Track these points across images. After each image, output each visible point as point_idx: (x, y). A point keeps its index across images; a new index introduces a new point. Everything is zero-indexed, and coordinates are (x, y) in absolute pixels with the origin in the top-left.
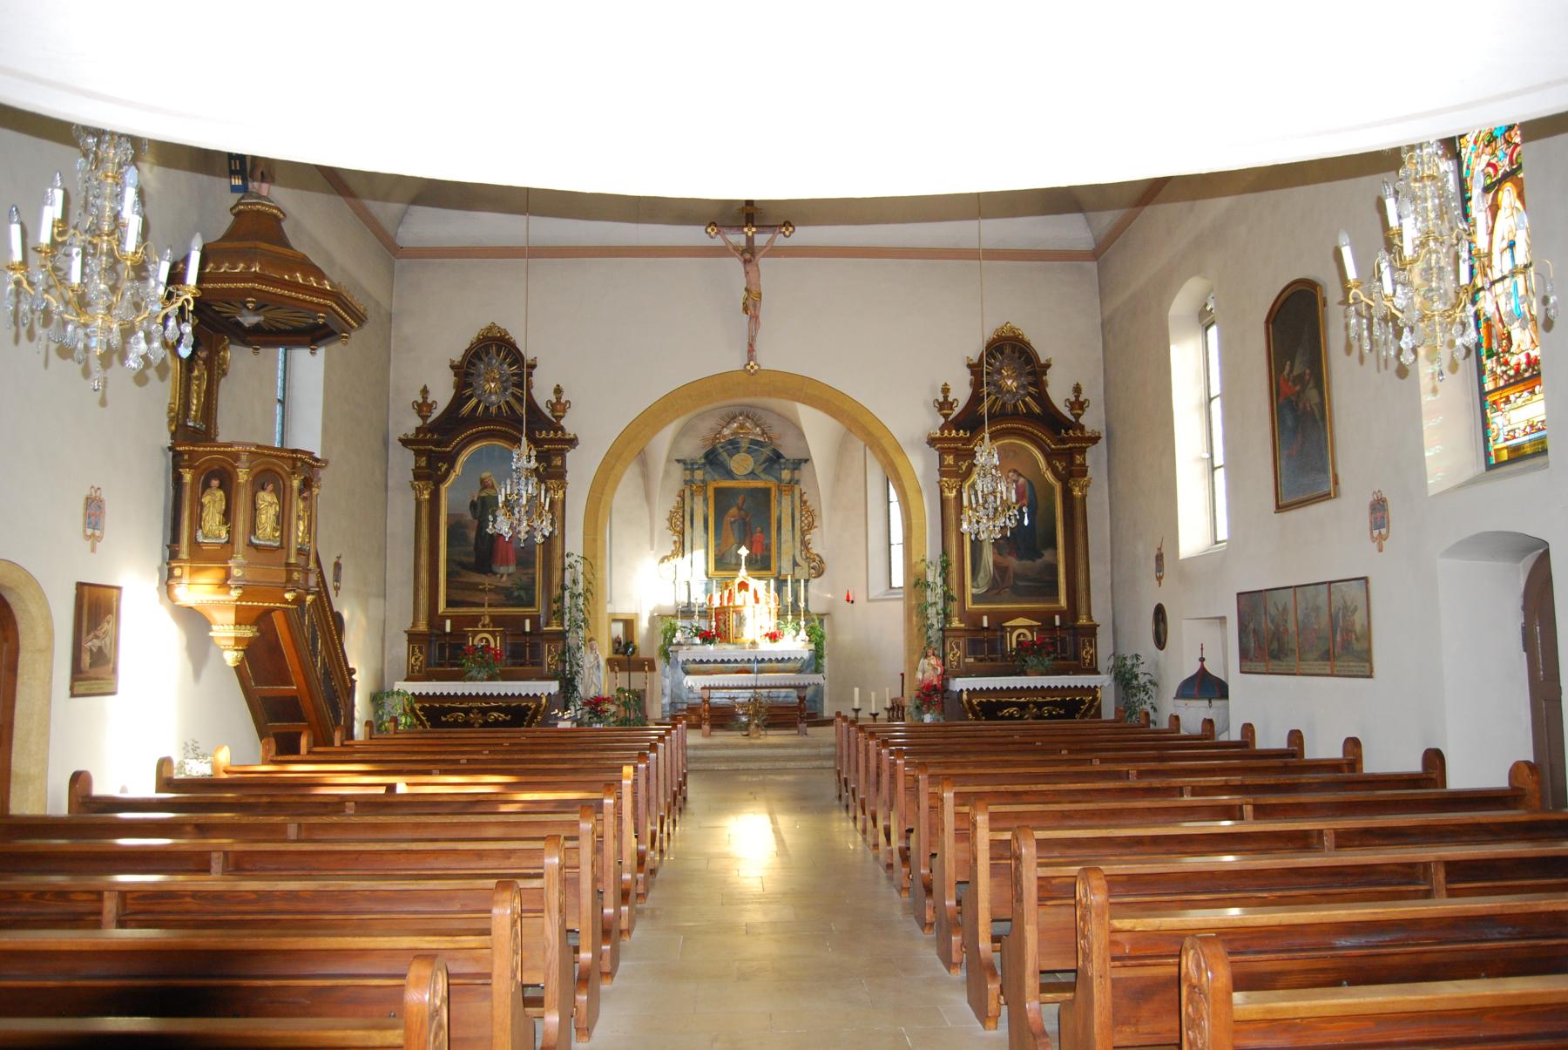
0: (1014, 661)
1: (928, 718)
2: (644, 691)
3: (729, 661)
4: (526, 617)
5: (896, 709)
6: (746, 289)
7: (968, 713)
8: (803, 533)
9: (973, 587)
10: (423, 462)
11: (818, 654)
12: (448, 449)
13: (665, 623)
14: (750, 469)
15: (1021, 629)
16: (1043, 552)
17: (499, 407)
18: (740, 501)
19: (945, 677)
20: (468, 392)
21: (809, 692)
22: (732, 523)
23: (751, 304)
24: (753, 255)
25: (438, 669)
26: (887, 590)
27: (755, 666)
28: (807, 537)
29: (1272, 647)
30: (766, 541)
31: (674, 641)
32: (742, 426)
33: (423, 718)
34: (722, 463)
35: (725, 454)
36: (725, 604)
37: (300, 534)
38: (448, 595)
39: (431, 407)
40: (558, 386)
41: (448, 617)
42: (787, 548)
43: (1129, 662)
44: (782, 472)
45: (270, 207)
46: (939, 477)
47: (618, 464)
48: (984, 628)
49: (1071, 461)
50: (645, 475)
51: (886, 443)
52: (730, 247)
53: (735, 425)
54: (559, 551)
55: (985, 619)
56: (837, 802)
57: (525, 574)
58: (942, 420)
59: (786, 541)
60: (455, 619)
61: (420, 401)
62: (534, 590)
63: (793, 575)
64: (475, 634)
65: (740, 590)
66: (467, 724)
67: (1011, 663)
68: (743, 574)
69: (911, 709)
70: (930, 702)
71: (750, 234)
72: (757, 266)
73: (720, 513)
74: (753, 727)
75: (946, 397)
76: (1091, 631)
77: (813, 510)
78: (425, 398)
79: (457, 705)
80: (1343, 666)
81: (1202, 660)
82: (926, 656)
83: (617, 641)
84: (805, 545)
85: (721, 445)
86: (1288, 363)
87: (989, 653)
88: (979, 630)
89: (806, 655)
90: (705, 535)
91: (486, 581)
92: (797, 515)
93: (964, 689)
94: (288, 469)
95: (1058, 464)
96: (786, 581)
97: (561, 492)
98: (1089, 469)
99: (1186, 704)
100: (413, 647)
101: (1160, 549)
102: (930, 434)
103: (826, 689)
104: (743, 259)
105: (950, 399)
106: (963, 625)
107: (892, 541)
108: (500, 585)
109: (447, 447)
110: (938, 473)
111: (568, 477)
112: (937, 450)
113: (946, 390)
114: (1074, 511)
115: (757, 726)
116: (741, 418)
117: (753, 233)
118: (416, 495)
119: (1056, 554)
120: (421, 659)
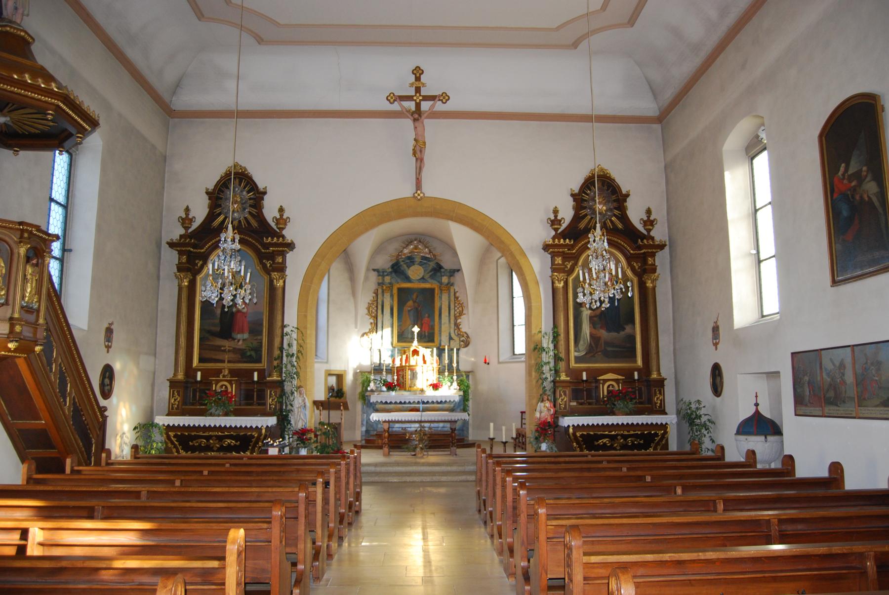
0: (606, 405)
1: (544, 446)
2: (340, 424)
3: (405, 403)
4: (256, 370)
5: (520, 440)
6: (415, 140)
7: (573, 443)
8: (456, 318)
9: (575, 351)
10: (184, 259)
11: (465, 398)
12: (202, 251)
13: (364, 377)
14: (421, 276)
15: (610, 382)
16: (626, 326)
17: (240, 222)
18: (414, 296)
19: (556, 416)
20: (218, 211)
21: (458, 426)
22: (409, 311)
23: (418, 151)
24: (420, 115)
25: (259, 407)
26: (511, 356)
27: (421, 406)
28: (459, 321)
29: (828, 396)
30: (431, 323)
31: (369, 389)
32: (416, 248)
33: (176, 443)
34: (403, 271)
35: (405, 266)
36: (404, 364)
37: (27, 295)
38: (200, 354)
39: (191, 221)
40: (281, 206)
41: (199, 370)
42: (445, 328)
43: (693, 406)
44: (443, 277)
45: (18, 29)
46: (551, 273)
47: (323, 262)
48: (583, 381)
49: (645, 262)
50: (352, 279)
51: (513, 248)
52: (404, 110)
53: (412, 246)
54: (279, 324)
55: (584, 374)
56: (477, 516)
57: (256, 340)
58: (553, 233)
59: (445, 323)
60: (205, 373)
61: (184, 216)
62: (261, 351)
63: (449, 346)
64: (217, 382)
65: (413, 355)
66: (209, 448)
67: (604, 406)
68: (415, 345)
69: (532, 440)
70: (545, 435)
71: (418, 101)
72: (423, 123)
73: (401, 304)
74: (418, 449)
75: (556, 217)
76: (661, 383)
77: (463, 303)
78: (187, 215)
79: (201, 434)
80: (872, 410)
81: (757, 405)
82: (543, 401)
83: (331, 389)
84: (457, 326)
85: (402, 259)
86: (843, 165)
87: (587, 399)
88: (580, 383)
89: (457, 399)
90: (391, 319)
91: (226, 344)
92: (452, 306)
93: (571, 425)
94: (16, 239)
95: (635, 264)
96: (444, 349)
97: (281, 282)
98: (658, 267)
99: (746, 439)
100: (173, 391)
101: (716, 323)
102: (545, 242)
103: (470, 422)
104: (412, 118)
105: (559, 218)
106: (568, 379)
107: (515, 324)
108: (238, 347)
109: (201, 249)
110: (550, 270)
111: (288, 272)
112: (550, 254)
113: (556, 212)
114: (647, 296)
115: (422, 449)
116: (415, 242)
117: (420, 95)
118: (179, 282)
119: (634, 328)
120: (178, 400)
